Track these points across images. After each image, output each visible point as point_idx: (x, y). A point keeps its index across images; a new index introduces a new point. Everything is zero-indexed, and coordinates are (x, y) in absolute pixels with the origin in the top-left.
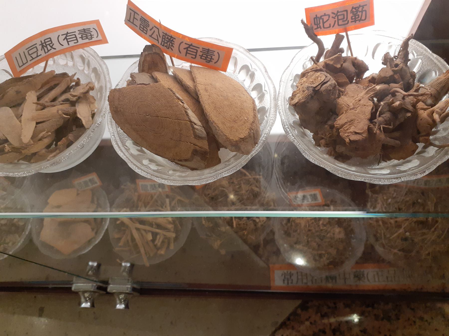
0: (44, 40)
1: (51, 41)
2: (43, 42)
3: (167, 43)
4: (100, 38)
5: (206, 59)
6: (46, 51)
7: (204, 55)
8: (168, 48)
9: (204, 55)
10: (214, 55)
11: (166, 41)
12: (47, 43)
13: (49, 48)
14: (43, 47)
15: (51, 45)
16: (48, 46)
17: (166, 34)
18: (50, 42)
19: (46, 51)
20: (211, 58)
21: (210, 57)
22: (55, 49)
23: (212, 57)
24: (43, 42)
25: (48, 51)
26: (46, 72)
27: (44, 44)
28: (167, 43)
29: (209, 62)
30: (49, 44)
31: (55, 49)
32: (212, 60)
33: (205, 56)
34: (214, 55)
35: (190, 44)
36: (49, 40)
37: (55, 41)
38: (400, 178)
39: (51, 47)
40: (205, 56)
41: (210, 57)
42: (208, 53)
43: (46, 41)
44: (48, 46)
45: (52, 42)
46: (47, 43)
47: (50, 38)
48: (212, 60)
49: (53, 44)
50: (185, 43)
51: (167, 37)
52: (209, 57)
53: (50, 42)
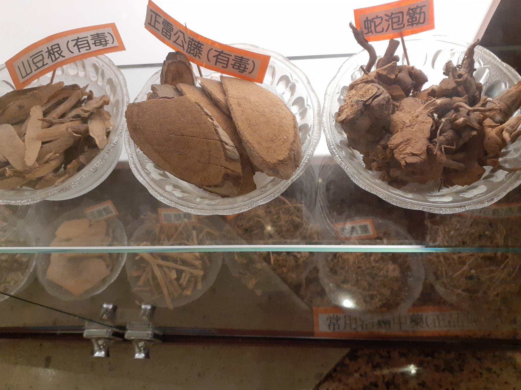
0: (52, 47)
1: (59, 47)
2: (50, 49)
3: (193, 50)
4: (116, 44)
5: (239, 69)
6: (54, 59)
7: (236, 64)
9: (236, 64)
10: (248, 64)
11: (192, 48)
12: (55, 50)
13: (57, 55)
14: (50, 54)
15: (59, 52)
16: (56, 53)
17: (193, 40)
18: (58, 49)
19: (54, 59)
20: (245, 68)
21: (244, 66)
22: (64, 57)
23: (246, 66)
24: (50, 49)
25: (56, 59)
27: (51, 52)
28: (193, 50)
29: (242, 72)
30: (57, 52)
31: (64, 57)
32: (246, 70)
33: (238, 65)
34: (248, 64)
35: (220, 51)
36: (57, 46)
37: (63, 47)
39: (60, 54)
40: (238, 65)
41: (244, 66)
42: (241, 62)
43: (54, 47)
44: (56, 53)
45: (60, 49)
46: (55, 50)
47: (58, 44)
48: (246, 70)
49: (62, 51)
50: (215, 50)
51: (193, 42)
52: (242, 66)
53: (58, 49)
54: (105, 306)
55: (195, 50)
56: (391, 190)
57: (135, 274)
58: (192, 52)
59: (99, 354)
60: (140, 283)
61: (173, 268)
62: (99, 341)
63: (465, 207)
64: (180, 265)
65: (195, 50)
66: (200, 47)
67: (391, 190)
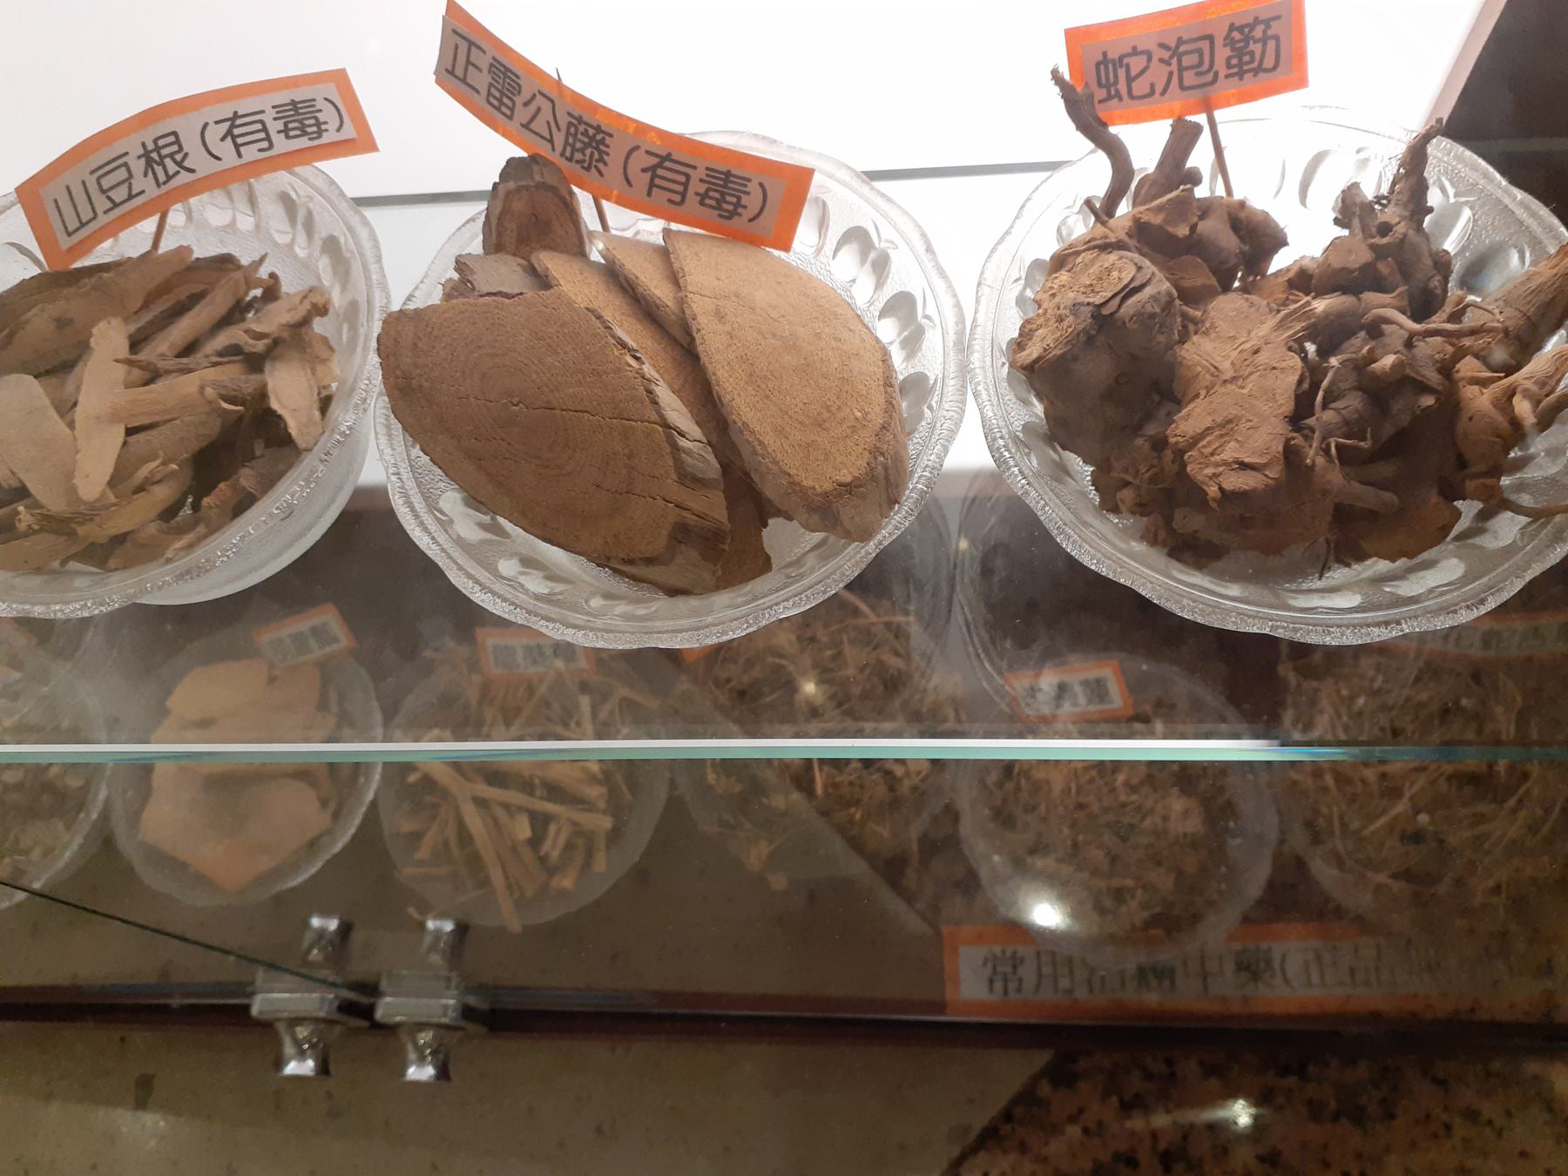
0: (155, 141)
1: (178, 142)
2: (150, 146)
3: (582, 151)
4: (349, 132)
5: (718, 207)
6: (162, 177)
7: (711, 194)
9: (711, 194)
10: (748, 193)
11: (578, 145)
12: (164, 152)
13: (172, 167)
14: (149, 163)
15: (178, 157)
16: (168, 161)
17: (580, 120)
18: (175, 148)
19: (162, 177)
20: (738, 204)
21: (734, 200)
22: (193, 171)
23: (739, 198)
24: (150, 146)
25: (169, 178)
26: (161, 251)
27: (154, 155)
28: (582, 151)
29: (729, 218)
30: (171, 156)
31: (193, 171)
32: (740, 210)
33: (717, 195)
34: (748, 193)
36: (172, 139)
37: (191, 143)
39: (179, 164)
40: (717, 195)
41: (734, 200)
42: (725, 186)
43: (161, 143)
44: (168, 161)
45: (181, 149)
46: (164, 152)
47: (174, 133)
48: (740, 210)
49: (186, 155)
50: (648, 152)
51: (582, 128)
52: (728, 198)
53: (175, 148)
54: (316, 922)
57: (407, 826)
59: (299, 1067)
60: (422, 854)
61: (521, 809)
62: (299, 1029)
63: (1398, 623)
64: (541, 798)
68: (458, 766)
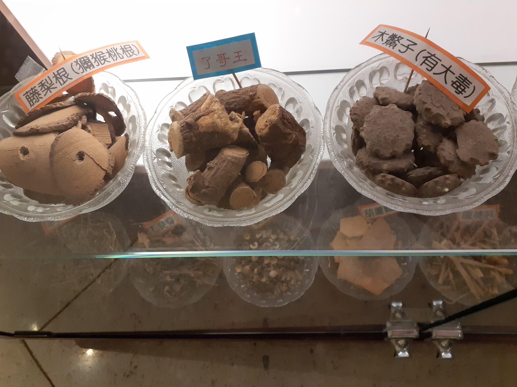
0: (57, 72)
1: (65, 70)
2: (56, 73)
3: (34, 98)
4: (141, 54)
5: (457, 89)
6: (62, 82)
7: (457, 83)
8: (39, 100)
9: (457, 83)
10: (469, 88)
11: (32, 98)
12: (61, 75)
13: (65, 79)
14: (57, 79)
15: (66, 75)
16: (63, 77)
17: (27, 93)
18: (64, 73)
19: (62, 82)
20: (463, 90)
21: (463, 88)
22: (71, 79)
23: (465, 88)
24: (56, 73)
25: (64, 82)
27: (58, 76)
28: (34, 98)
29: (458, 94)
30: (64, 75)
31: (71, 79)
32: (463, 92)
33: (458, 84)
34: (469, 88)
35: (433, 54)
36: (63, 70)
37: (68, 70)
38: (508, 175)
39: (67, 77)
40: (458, 84)
41: (463, 88)
42: (463, 82)
43: (59, 72)
44: (63, 77)
45: (66, 73)
46: (61, 75)
47: (63, 68)
48: (463, 92)
49: (68, 74)
50: (428, 52)
51: (29, 94)
52: (461, 87)
53: (64, 73)
54: (394, 305)
55: (35, 97)
56: (237, 215)
57: (434, 273)
58: (34, 101)
59: (403, 354)
60: (440, 281)
61: (476, 267)
62: (399, 342)
64: (485, 263)
65: (35, 97)
66: (35, 90)
67: (237, 215)
68: (458, 256)
